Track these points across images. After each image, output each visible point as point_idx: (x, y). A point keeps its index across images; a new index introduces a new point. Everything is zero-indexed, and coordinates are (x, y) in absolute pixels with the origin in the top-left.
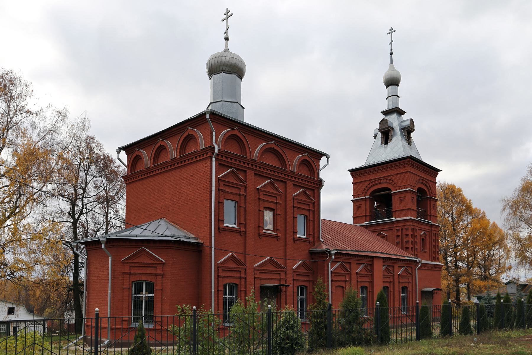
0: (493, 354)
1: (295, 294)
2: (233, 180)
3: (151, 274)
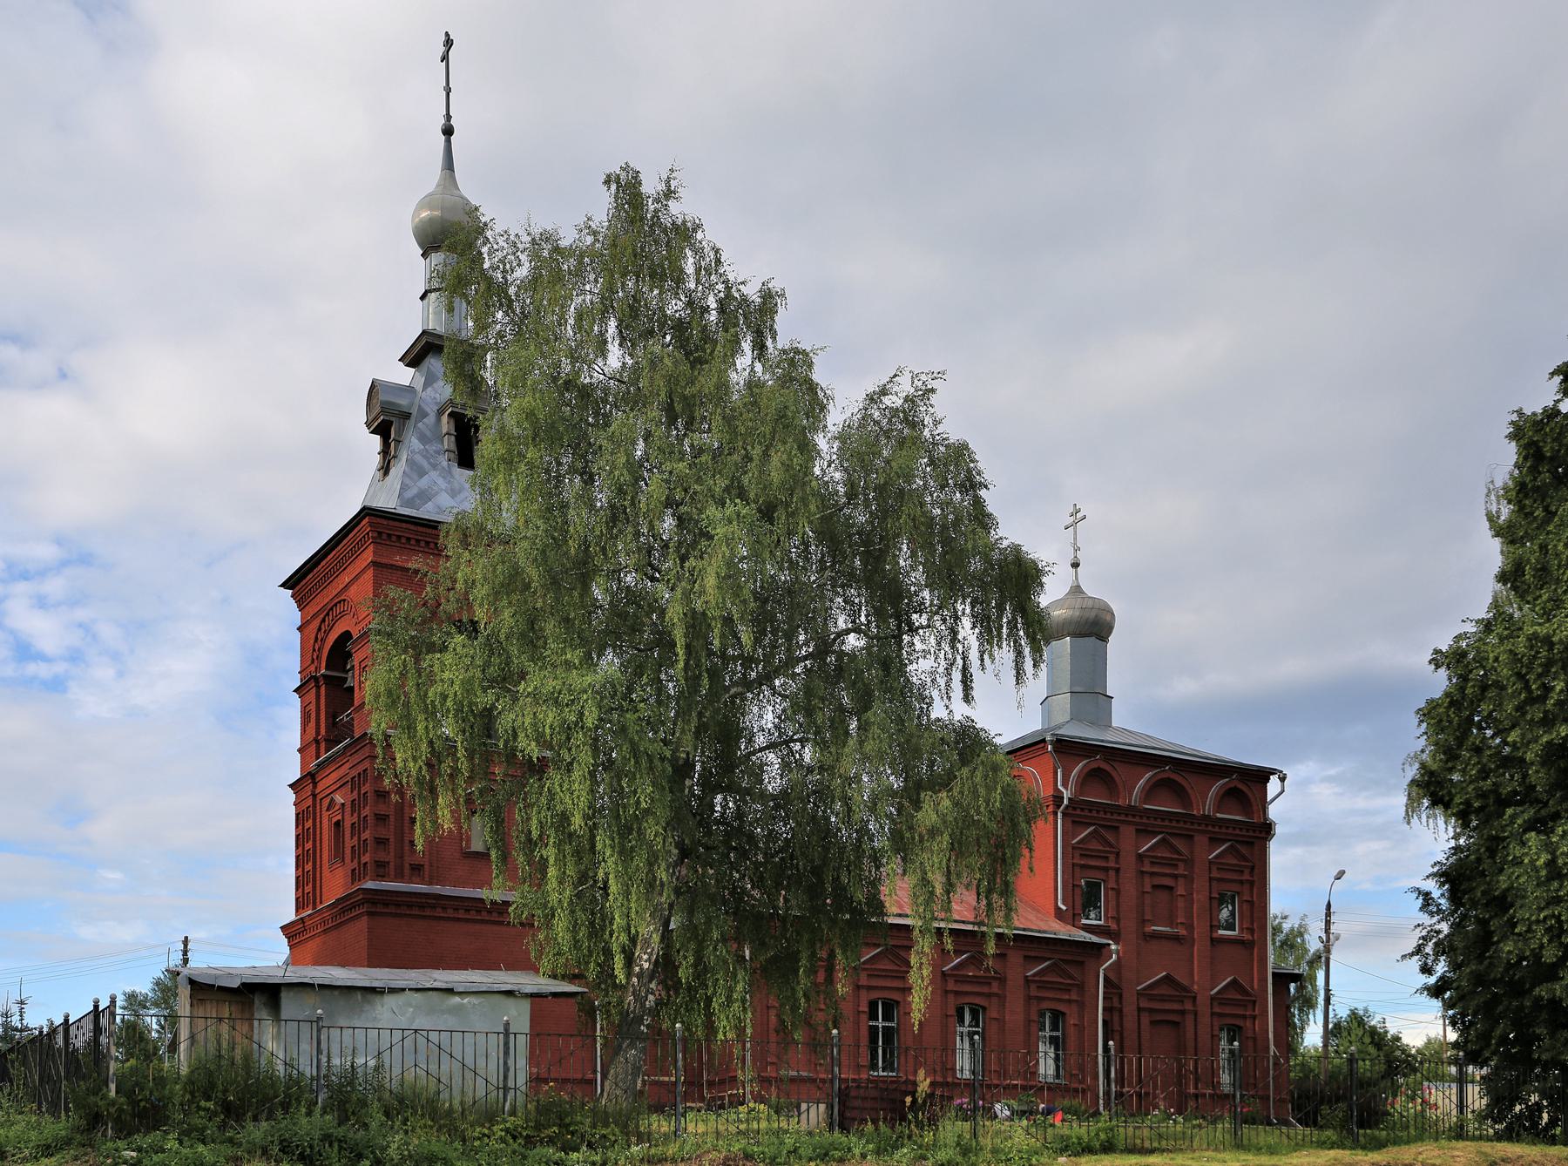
0: (432, 1159)
1: (1034, 1027)
2: (1095, 845)
3: (1173, 1011)
